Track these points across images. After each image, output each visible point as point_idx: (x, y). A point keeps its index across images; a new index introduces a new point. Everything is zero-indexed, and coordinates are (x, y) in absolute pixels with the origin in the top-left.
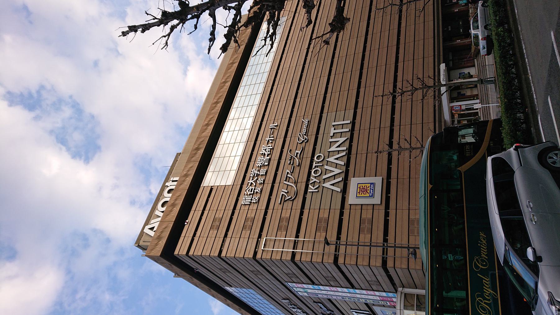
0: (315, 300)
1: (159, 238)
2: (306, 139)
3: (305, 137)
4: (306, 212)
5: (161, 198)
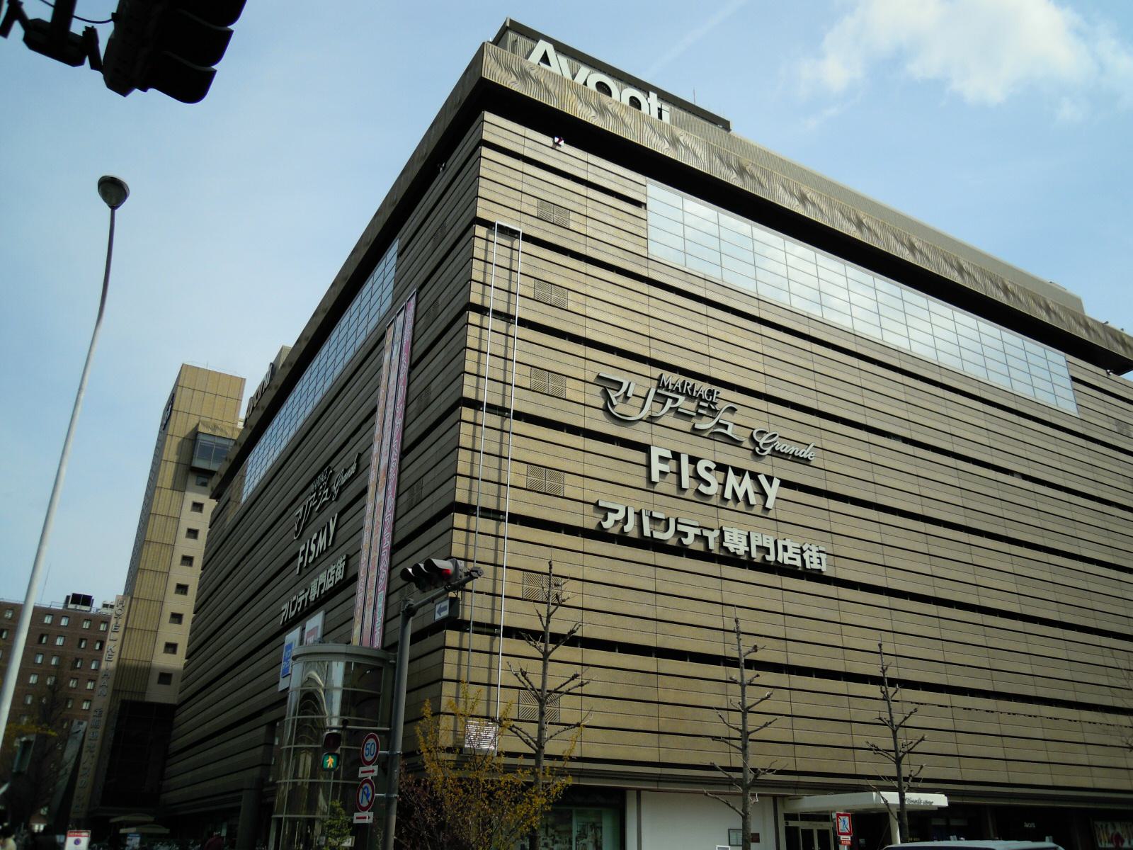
0: (363, 458)
1: (524, 75)
2: (762, 451)
3: (768, 450)
4: (578, 441)
5: (620, 83)
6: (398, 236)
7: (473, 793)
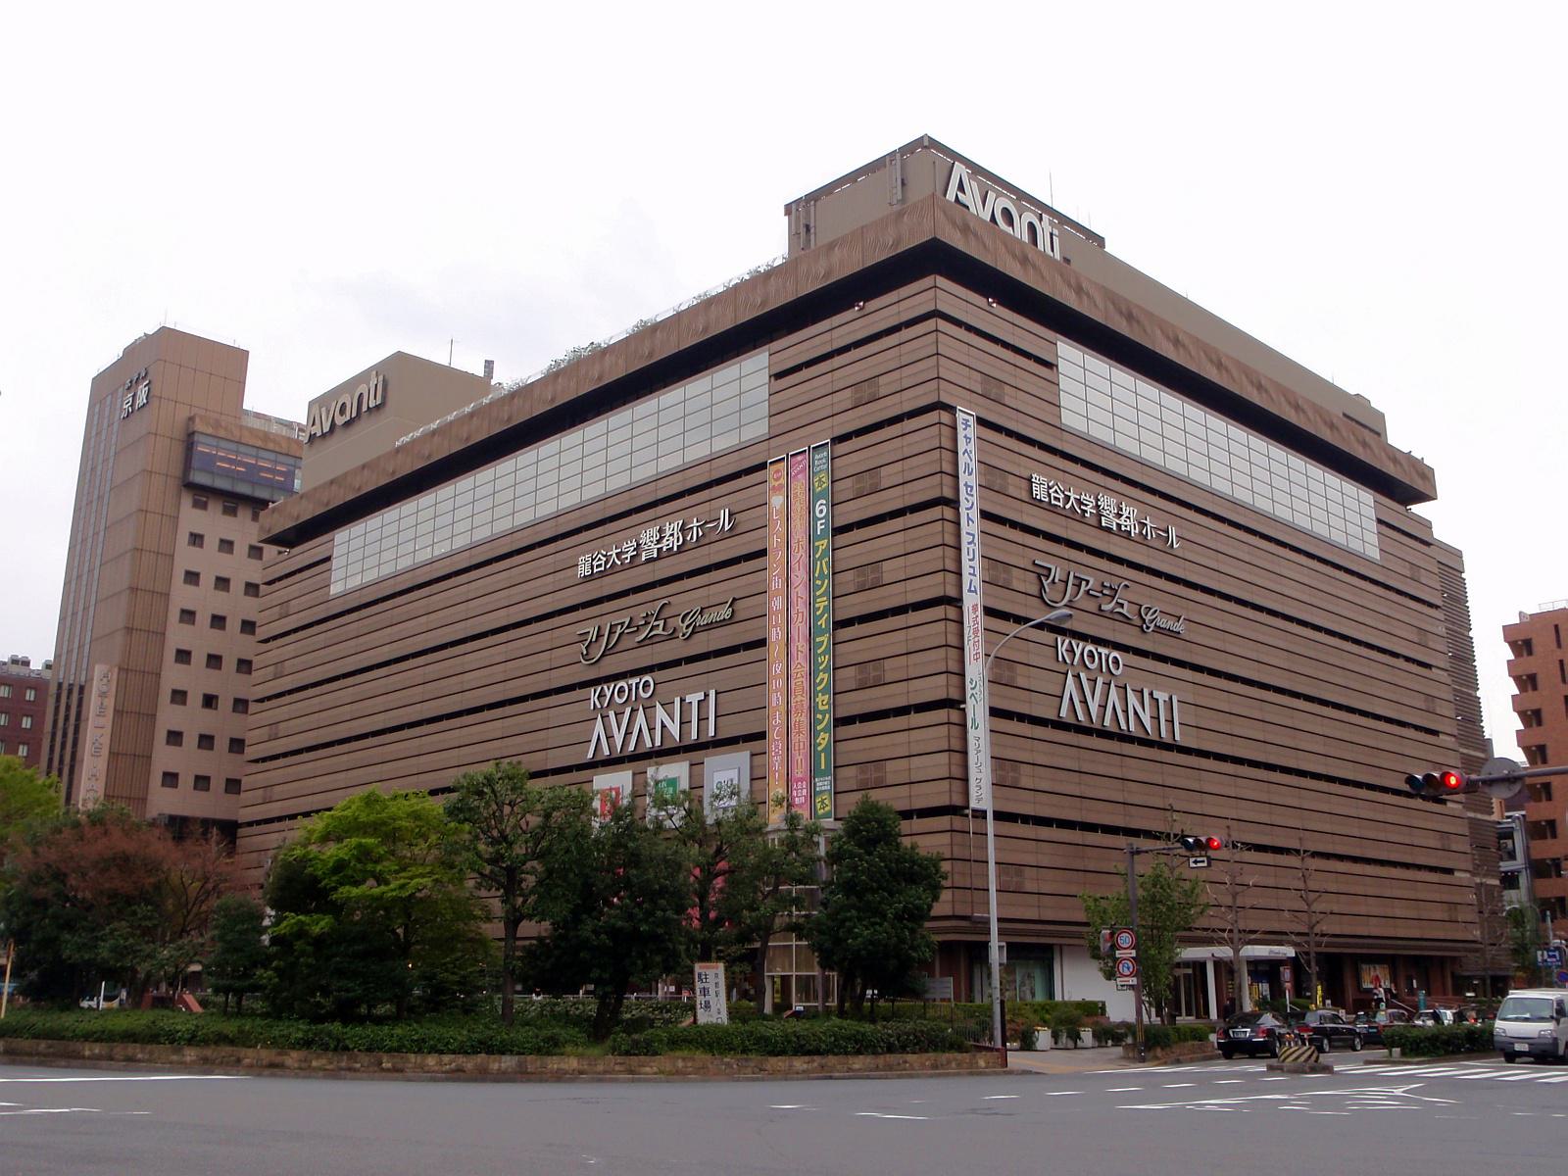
6: (776, 345)
7: (1549, 956)
